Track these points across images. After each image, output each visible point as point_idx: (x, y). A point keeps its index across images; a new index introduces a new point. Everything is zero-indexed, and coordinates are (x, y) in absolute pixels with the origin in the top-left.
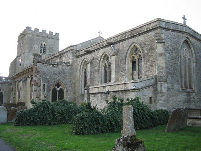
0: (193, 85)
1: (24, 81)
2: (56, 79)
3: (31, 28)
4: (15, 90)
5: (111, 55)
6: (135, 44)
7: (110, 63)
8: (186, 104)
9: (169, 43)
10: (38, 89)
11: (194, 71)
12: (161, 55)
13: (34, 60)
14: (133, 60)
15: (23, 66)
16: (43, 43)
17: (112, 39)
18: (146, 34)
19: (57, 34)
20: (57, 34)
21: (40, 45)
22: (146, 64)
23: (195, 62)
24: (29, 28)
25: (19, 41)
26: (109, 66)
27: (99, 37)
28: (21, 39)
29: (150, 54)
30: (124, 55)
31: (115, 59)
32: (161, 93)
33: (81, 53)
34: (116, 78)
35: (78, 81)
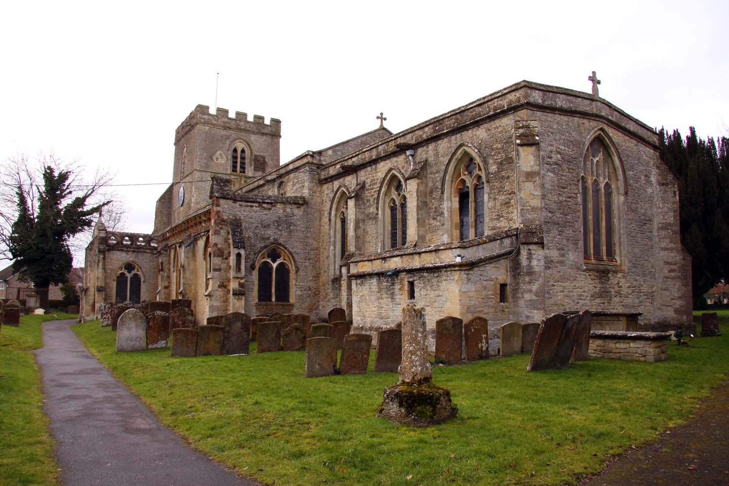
0: (617, 251)
1: (189, 245)
2: (269, 238)
3: (208, 108)
4: (169, 270)
5: (406, 176)
6: (466, 148)
7: (405, 198)
8: (598, 301)
9: (552, 146)
10: (223, 266)
11: (619, 214)
12: (530, 176)
13: (212, 192)
14: (460, 189)
15: (190, 207)
16: (240, 146)
17: (409, 136)
18: (492, 123)
19: (276, 123)
20: (276, 123)
21: (230, 153)
22: (495, 199)
23: (622, 191)
24: (202, 109)
25: (177, 142)
26: (403, 206)
27: (379, 130)
28: (183, 136)
29: (503, 174)
30: (439, 177)
31: (415, 187)
32: (530, 272)
33: (331, 172)
34: (418, 234)
35: (325, 245)
